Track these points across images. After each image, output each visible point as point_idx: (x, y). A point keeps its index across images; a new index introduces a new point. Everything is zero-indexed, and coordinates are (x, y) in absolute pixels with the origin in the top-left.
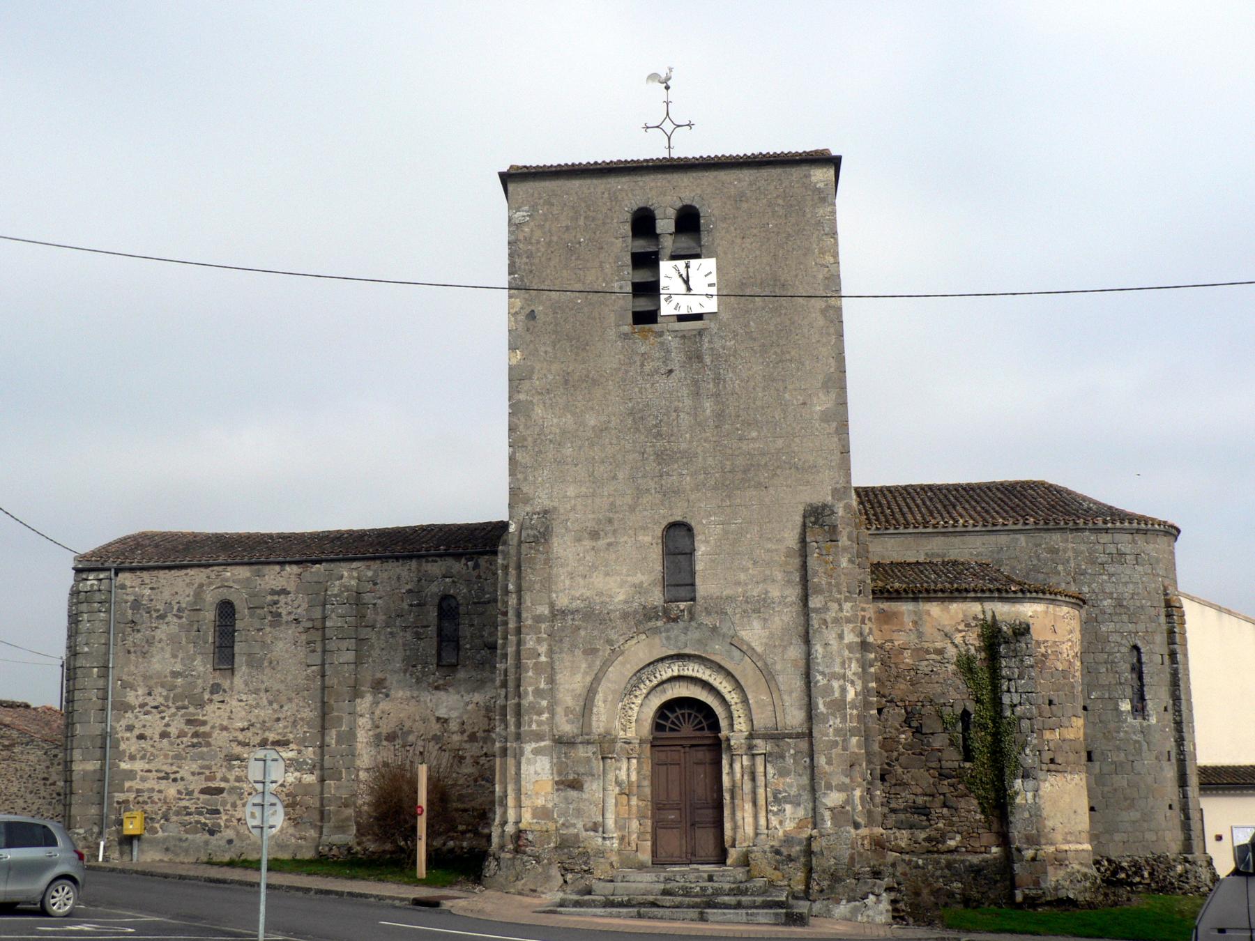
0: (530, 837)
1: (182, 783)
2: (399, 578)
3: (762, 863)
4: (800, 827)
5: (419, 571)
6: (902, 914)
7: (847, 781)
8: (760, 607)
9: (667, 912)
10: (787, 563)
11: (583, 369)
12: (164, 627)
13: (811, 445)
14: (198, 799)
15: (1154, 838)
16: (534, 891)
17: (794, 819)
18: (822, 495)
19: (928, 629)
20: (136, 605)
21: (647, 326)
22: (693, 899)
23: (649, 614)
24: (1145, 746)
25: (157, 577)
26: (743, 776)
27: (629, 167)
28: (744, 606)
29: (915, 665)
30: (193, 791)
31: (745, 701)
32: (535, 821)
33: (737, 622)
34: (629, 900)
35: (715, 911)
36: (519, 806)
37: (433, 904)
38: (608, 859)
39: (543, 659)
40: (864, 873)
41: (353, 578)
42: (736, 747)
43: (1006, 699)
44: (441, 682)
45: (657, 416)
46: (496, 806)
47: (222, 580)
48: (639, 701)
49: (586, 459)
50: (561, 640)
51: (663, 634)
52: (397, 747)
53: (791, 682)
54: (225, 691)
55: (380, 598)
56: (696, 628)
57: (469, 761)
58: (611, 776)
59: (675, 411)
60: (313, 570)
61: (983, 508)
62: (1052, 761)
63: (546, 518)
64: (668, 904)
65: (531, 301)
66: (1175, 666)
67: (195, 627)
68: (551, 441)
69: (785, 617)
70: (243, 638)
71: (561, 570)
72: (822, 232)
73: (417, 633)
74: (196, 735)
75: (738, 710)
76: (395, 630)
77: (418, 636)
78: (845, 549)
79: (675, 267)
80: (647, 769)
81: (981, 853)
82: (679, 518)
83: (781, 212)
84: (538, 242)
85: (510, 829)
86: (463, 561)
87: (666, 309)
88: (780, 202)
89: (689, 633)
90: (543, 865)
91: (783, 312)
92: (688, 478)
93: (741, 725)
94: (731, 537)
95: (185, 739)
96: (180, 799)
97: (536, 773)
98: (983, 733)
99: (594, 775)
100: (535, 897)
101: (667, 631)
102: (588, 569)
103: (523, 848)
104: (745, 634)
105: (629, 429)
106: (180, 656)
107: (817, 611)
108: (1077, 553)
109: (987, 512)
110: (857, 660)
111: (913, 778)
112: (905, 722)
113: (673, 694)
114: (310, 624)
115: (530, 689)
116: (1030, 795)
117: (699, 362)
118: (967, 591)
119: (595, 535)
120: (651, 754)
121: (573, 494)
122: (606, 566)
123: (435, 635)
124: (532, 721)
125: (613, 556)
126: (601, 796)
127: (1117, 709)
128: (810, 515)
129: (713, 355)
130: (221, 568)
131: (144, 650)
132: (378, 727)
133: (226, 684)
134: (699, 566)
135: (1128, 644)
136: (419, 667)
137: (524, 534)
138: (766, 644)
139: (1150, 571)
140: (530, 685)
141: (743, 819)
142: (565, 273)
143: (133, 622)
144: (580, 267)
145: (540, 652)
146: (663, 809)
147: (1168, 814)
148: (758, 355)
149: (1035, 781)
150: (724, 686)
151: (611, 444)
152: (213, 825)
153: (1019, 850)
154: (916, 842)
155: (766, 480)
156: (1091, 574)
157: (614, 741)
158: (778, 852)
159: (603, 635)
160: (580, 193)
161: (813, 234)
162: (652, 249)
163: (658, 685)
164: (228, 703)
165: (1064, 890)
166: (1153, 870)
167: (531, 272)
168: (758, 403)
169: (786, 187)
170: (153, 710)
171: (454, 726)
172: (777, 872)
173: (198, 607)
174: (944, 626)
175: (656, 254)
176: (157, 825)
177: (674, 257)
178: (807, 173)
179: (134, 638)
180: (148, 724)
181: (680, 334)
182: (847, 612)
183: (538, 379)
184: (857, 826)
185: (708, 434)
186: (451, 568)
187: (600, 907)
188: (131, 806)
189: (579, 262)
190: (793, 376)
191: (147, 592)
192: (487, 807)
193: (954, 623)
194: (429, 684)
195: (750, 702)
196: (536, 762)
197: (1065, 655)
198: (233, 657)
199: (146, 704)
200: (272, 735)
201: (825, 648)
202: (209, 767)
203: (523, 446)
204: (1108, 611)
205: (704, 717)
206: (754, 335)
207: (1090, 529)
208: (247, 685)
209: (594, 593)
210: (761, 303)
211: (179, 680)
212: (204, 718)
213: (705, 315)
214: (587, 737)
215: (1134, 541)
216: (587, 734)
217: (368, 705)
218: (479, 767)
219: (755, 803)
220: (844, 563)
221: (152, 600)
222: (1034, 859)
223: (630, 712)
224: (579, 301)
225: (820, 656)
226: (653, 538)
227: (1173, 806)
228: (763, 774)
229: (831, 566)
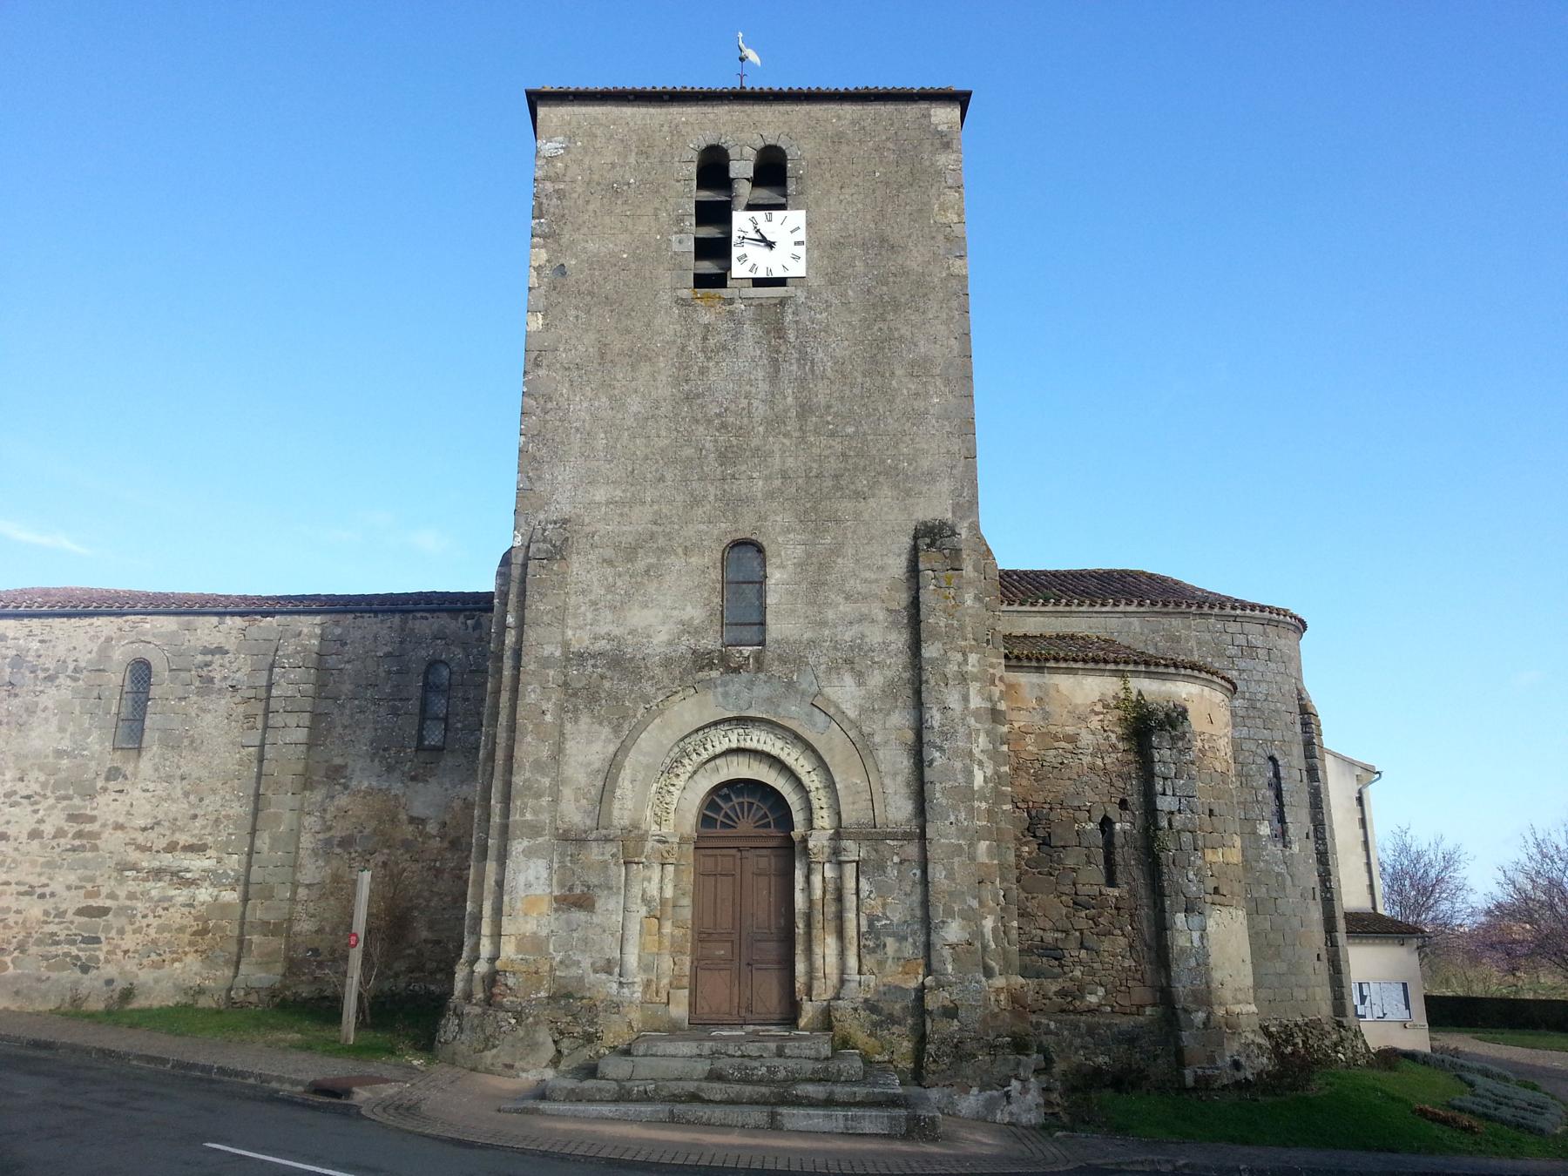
0: (511, 981)
3: (854, 1025)
5: (403, 630)
9: (718, 1113)
12: (52, 691)
14: (72, 922)
15: (1303, 997)
16: (511, 1067)
17: (899, 959)
21: (712, 291)
22: (757, 1088)
23: (703, 661)
28: (832, 654)
31: (831, 785)
32: (520, 956)
33: (821, 675)
36: (497, 935)
42: (815, 851)
45: (722, 403)
47: (137, 633)
48: (680, 782)
51: (720, 689)
52: (353, 855)
53: (896, 761)
54: (125, 777)
55: (348, 662)
56: (765, 682)
58: (636, 890)
60: (261, 624)
62: (1216, 890)
63: (565, 529)
64: (718, 1097)
67: (95, 694)
68: (578, 430)
74: (79, 835)
75: (820, 799)
77: (395, 712)
79: (753, 220)
80: (688, 879)
83: (892, 157)
85: (481, 967)
86: (461, 618)
87: (738, 270)
88: (891, 146)
90: (526, 1025)
93: (824, 819)
95: (62, 841)
96: (46, 922)
101: (725, 684)
106: (71, 729)
107: (932, 661)
110: (988, 733)
112: (1028, 829)
113: (729, 775)
114: (252, 693)
116: (1196, 935)
118: (1106, 662)
124: (526, 808)
126: (621, 920)
131: (21, 721)
133: (129, 769)
134: (771, 600)
137: (533, 548)
139: (1283, 670)
142: (607, 219)
143: (11, 684)
144: (628, 213)
146: (709, 941)
147: (1317, 967)
150: (801, 764)
152: (90, 958)
154: (1044, 997)
157: (643, 838)
160: (632, 124)
163: (709, 761)
164: (128, 793)
167: (563, 216)
169: (898, 129)
170: (23, 801)
171: (432, 828)
175: (729, 203)
176: (8, 959)
179: (9, 705)
180: (13, 820)
181: (755, 302)
182: (973, 666)
184: (988, 973)
185: (789, 428)
189: (626, 207)
191: (35, 645)
194: (403, 773)
195: (838, 786)
198: (142, 735)
199: (15, 793)
200: (184, 837)
202: (92, 879)
205: (770, 809)
208: (157, 770)
209: (626, 632)
211: (65, 761)
212: (95, 813)
215: (1265, 634)
219: (841, 934)
220: (969, 599)
221: (39, 656)
222: (1206, 1023)
223: (668, 799)
224: (625, 256)
227: (1321, 957)
228: (854, 891)
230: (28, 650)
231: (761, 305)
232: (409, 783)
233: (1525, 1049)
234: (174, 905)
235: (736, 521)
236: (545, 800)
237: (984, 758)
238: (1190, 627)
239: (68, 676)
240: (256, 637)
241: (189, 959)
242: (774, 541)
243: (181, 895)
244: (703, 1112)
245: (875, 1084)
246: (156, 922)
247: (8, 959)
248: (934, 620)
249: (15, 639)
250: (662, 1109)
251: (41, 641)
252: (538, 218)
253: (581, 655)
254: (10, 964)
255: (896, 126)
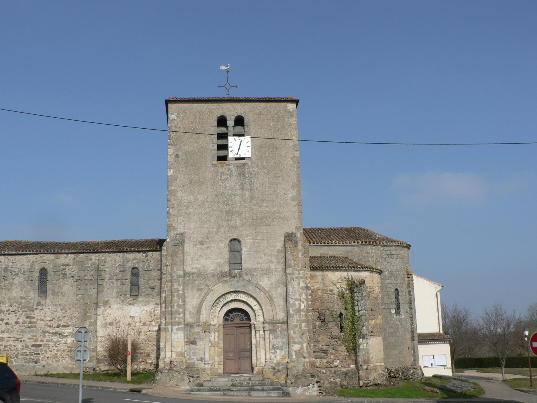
0: (175, 364)
1: (24, 342)
2: (115, 260)
3: (269, 374)
4: (283, 359)
5: (123, 258)
6: (322, 391)
7: (301, 340)
8: (267, 272)
9: (236, 393)
10: (277, 255)
11: (197, 178)
12: (17, 279)
13: (287, 210)
14: (31, 349)
15: (403, 360)
16: (177, 385)
18: (291, 229)
19: (327, 282)
20: (6, 269)
21: (223, 162)
22: (245, 387)
23: (223, 275)
24: (400, 326)
25: (15, 258)
26: (260, 338)
27: (217, 100)
28: (261, 272)
29: (323, 296)
30: (28, 346)
32: (177, 357)
34: (219, 388)
35: (255, 392)
37: (138, 391)
38: (207, 372)
39: (181, 292)
40: (308, 376)
41: (97, 260)
43: (357, 309)
44: (132, 302)
48: (219, 309)
49: (199, 213)
50: (188, 285)
51: (229, 283)
53: (279, 302)
55: (107, 268)
56: (242, 281)
57: (143, 333)
59: (234, 195)
60: (80, 256)
61: (341, 237)
64: (235, 390)
65: (177, 150)
66: (410, 296)
67: (31, 279)
68: (184, 206)
69: (277, 277)
70: (51, 284)
71: (188, 257)
72: (292, 128)
73: (122, 282)
74: (30, 323)
76: (113, 281)
77: (123, 284)
78: (300, 250)
80: (221, 337)
81: (347, 367)
82: (235, 237)
83: (276, 119)
84: (180, 127)
87: (231, 155)
88: (276, 116)
89: (239, 282)
91: (276, 158)
92: (239, 222)
94: (256, 245)
96: (23, 349)
97: (178, 338)
98: (348, 322)
99: (201, 339)
100: (177, 388)
101: (230, 281)
102: (198, 256)
103: (172, 368)
104: (261, 283)
105: (216, 202)
106: (24, 290)
107: (290, 274)
108: (376, 254)
109: (342, 238)
111: (321, 339)
112: (318, 317)
114: (78, 278)
115: (175, 304)
116: (365, 345)
117: (244, 176)
119: (201, 243)
120: (223, 330)
121: (193, 227)
122: (206, 256)
123: (130, 283)
124: (176, 317)
125: (209, 252)
127: (390, 312)
128: (287, 237)
129: (249, 174)
130: (42, 255)
131: (9, 288)
132: (106, 320)
133: (43, 302)
134: (243, 256)
135: (394, 288)
136: (123, 296)
138: (270, 287)
139: (401, 261)
140: (175, 303)
141: (260, 355)
142: (191, 140)
143: (4, 276)
145: (179, 289)
148: (267, 174)
149: (367, 340)
151: (208, 207)
153: (361, 366)
155: (270, 223)
156: (381, 262)
157: (210, 325)
158: (274, 368)
159: (205, 283)
161: (288, 128)
162: (226, 131)
166: (403, 372)
168: (267, 193)
171: (137, 319)
172: (274, 376)
173: (32, 271)
174: (333, 281)
175: (227, 134)
176: (13, 360)
177: (234, 135)
178: (286, 105)
180: (10, 318)
181: (237, 165)
182: (301, 275)
183: (179, 181)
184: (305, 358)
185: (247, 205)
186: (137, 256)
187: (207, 392)
188: (2, 352)
190: (280, 183)
191: (11, 264)
192: (150, 352)
193: (337, 280)
196: (178, 333)
197: (376, 292)
198: (46, 291)
199: (9, 310)
201: (293, 289)
202: (35, 336)
203: (173, 208)
204: (387, 276)
206: (265, 166)
207: (381, 245)
209: (202, 266)
210: (268, 154)
212: (34, 316)
214: (198, 324)
215: (396, 250)
216: (198, 323)
217: (102, 311)
218: (147, 336)
220: (300, 255)
221: (12, 268)
222: (367, 369)
223: (215, 314)
224: (196, 151)
225: (291, 292)
226: (225, 245)
228: (268, 338)
229: (295, 257)
230: (9, 266)
231: (238, 166)
232: (129, 306)
234: (61, 343)
235: (232, 233)
236: (182, 315)
237: (304, 300)
238: (373, 249)
239: (22, 274)
240: (78, 260)
241: (67, 359)
242: (244, 239)
243: (63, 340)
244: (232, 393)
245: (274, 386)
246: (56, 348)
247: (13, 360)
248: (291, 262)
249: (4, 262)
250: (222, 393)
251: (13, 263)
252: (170, 139)
253: (189, 274)
254: (14, 361)
255: (277, 109)
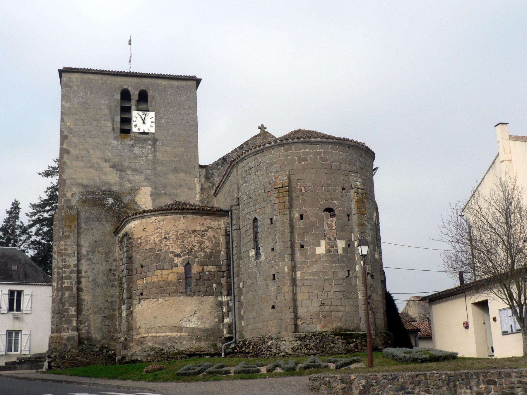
46: (67, 325)
87: (134, 129)
165: (136, 356)
213: (149, 134)
233: (109, 384)
